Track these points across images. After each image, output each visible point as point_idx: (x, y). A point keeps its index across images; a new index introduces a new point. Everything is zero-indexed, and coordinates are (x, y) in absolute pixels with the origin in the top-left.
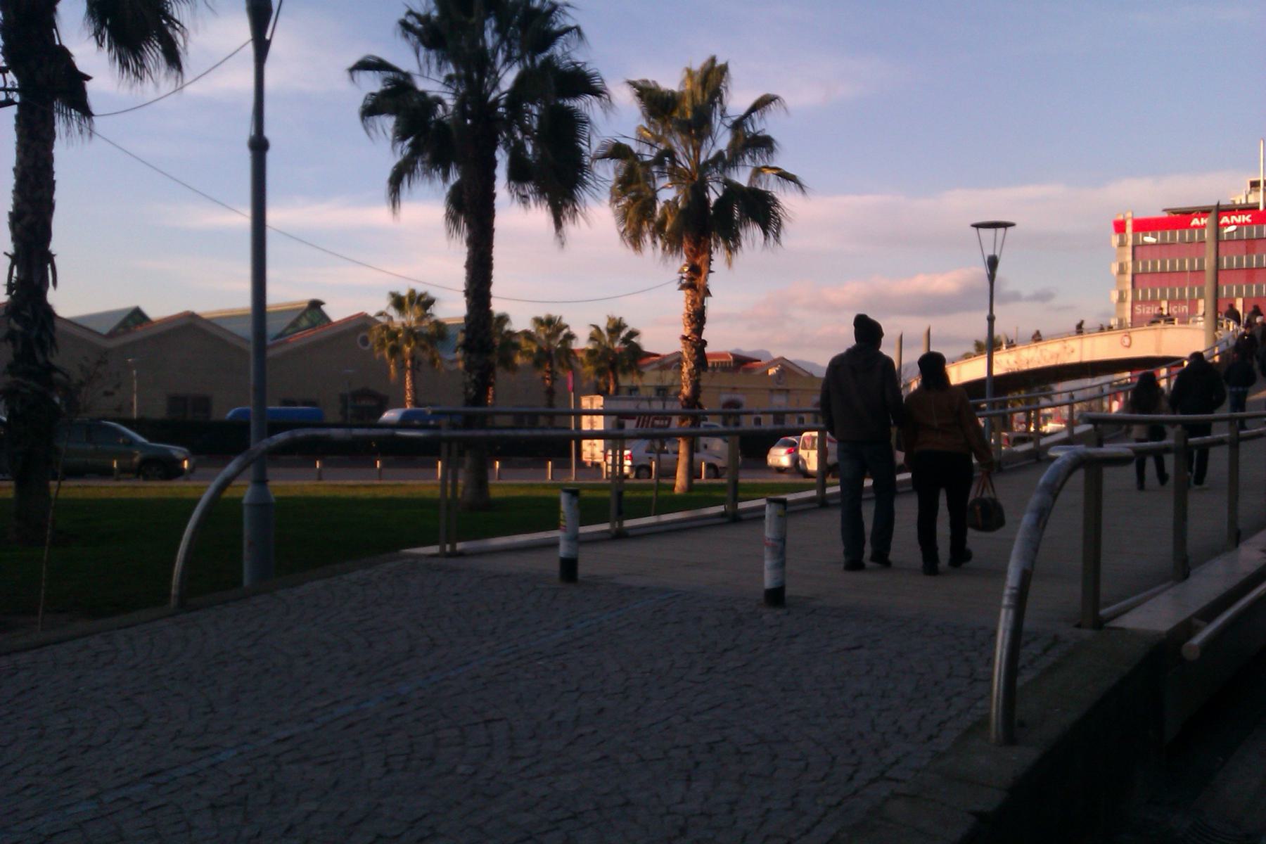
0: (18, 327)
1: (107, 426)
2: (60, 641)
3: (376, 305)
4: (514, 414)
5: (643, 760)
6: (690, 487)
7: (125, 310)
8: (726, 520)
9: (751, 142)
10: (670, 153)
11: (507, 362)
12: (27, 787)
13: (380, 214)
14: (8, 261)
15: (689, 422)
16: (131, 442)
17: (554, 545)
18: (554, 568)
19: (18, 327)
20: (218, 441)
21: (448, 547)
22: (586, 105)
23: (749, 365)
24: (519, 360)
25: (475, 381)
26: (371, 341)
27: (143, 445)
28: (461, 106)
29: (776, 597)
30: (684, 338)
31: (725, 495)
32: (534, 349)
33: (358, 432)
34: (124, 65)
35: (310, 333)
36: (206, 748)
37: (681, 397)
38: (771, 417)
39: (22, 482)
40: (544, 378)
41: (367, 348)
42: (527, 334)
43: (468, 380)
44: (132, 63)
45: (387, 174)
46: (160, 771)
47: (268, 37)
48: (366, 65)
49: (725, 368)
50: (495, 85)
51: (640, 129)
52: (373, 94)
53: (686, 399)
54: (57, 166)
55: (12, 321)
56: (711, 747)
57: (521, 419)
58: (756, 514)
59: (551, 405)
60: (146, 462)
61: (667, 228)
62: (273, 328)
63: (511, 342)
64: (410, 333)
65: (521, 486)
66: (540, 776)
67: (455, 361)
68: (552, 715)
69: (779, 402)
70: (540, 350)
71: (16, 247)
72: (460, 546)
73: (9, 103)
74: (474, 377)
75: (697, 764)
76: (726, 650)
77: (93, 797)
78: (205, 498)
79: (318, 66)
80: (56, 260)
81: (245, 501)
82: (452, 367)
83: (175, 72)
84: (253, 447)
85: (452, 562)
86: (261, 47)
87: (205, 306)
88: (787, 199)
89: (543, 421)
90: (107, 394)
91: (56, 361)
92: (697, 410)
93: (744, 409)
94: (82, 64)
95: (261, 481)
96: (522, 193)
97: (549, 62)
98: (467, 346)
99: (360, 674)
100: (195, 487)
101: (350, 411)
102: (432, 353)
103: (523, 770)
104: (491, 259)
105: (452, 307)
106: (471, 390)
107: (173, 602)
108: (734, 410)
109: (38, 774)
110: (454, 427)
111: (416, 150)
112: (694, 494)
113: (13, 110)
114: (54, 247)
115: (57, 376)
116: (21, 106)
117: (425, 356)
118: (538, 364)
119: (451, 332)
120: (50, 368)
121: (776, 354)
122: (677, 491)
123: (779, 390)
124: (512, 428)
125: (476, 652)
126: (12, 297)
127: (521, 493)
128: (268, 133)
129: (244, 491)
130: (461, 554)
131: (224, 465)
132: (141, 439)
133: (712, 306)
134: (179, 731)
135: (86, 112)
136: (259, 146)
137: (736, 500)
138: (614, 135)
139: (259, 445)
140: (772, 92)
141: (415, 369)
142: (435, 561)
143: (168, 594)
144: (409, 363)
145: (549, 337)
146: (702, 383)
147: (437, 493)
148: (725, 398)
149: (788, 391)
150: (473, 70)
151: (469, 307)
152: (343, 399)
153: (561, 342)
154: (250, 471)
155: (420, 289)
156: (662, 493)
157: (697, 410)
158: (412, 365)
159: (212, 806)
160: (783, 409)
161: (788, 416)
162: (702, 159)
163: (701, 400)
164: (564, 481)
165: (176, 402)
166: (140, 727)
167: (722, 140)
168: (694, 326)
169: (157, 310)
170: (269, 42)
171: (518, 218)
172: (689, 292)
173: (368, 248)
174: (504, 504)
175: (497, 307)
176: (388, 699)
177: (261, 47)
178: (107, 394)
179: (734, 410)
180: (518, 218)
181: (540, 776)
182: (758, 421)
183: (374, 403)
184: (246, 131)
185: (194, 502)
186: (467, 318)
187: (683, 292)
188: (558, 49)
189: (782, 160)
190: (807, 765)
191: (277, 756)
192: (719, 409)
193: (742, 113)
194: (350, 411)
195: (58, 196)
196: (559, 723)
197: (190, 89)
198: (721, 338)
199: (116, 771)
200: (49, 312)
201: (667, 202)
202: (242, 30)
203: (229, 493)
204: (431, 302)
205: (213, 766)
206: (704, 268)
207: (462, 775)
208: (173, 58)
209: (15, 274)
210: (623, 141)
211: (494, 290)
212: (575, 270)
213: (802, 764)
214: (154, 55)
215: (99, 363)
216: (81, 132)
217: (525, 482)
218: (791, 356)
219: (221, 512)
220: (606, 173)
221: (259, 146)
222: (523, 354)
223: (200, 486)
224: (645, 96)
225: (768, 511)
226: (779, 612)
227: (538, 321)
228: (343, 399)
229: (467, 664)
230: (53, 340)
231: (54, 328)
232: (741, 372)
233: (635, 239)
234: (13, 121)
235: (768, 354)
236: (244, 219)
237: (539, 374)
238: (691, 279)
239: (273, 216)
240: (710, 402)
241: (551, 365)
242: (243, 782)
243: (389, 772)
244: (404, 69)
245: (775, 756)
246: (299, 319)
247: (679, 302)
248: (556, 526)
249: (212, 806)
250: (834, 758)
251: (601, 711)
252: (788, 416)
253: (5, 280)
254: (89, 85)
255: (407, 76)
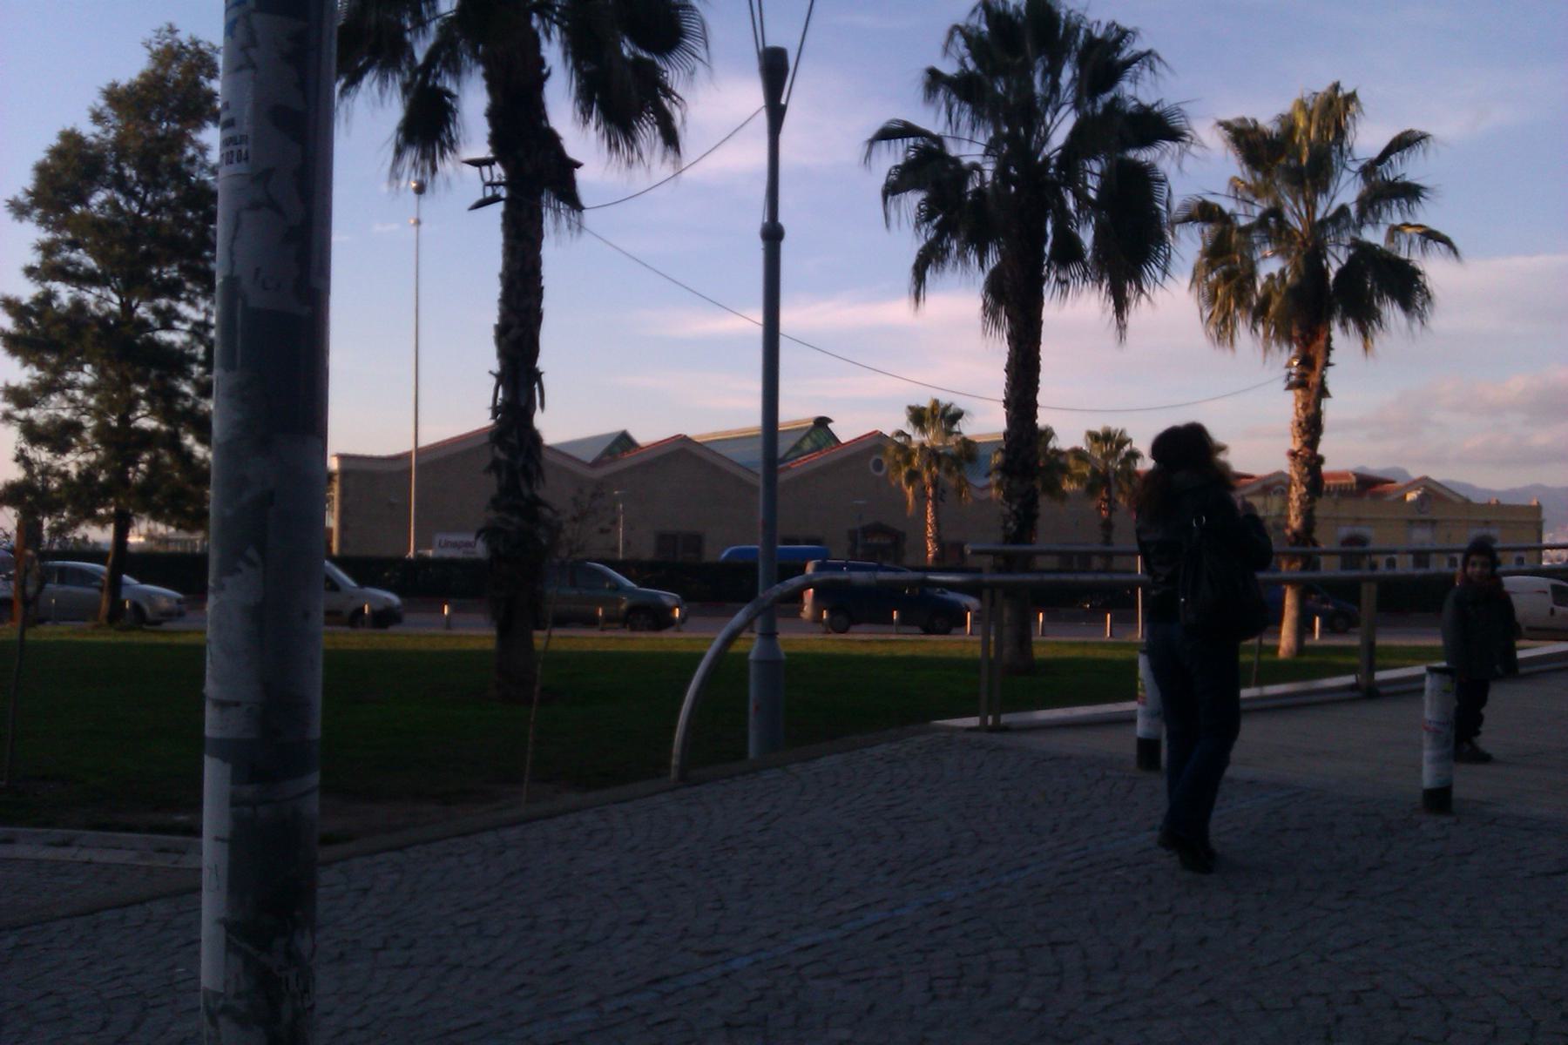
0: (502, 456)
1: (596, 571)
2: (550, 816)
3: (894, 422)
4: (1059, 553)
5: (1264, 1009)
6: (1300, 649)
7: (609, 435)
8: (1356, 694)
9: (1386, 191)
10: (1276, 212)
11: (1053, 489)
12: (522, 986)
13: (899, 310)
14: (493, 381)
15: (1299, 564)
16: (618, 587)
17: (1130, 720)
18: (1131, 750)
19: (502, 456)
20: (720, 586)
21: (990, 720)
22: (1160, 157)
23: (1379, 489)
24: (1069, 486)
25: (1015, 512)
26: (885, 463)
27: (631, 590)
28: (1001, 172)
29: (1439, 800)
30: (1293, 454)
31: (1354, 661)
32: (1086, 470)
33: (882, 576)
34: (613, 146)
35: (816, 457)
36: (719, 952)
37: (1288, 532)
38: (1410, 557)
39: (506, 629)
40: (1099, 508)
41: (882, 473)
42: (1077, 453)
43: (1007, 511)
44: (623, 145)
45: (911, 260)
46: (667, 978)
47: (783, 102)
48: (888, 134)
49: (1344, 492)
50: (1045, 141)
51: (1234, 183)
52: (896, 167)
53: (1295, 534)
54: (546, 271)
55: (497, 449)
56: (1356, 998)
57: (1066, 557)
58: (1415, 686)
59: (1107, 540)
60: (633, 610)
61: (1272, 309)
62: (784, 446)
63: (1059, 463)
64: (933, 455)
65: (1072, 645)
66: (1127, 1019)
67: (989, 487)
68: (1138, 941)
69: (1421, 537)
70: (1095, 472)
71: (503, 367)
72: (1005, 719)
73: (495, 199)
74: (1014, 507)
75: (1339, 1019)
76: (1370, 869)
77: (591, 1004)
78: (710, 653)
79: (838, 131)
80: (544, 378)
81: (751, 657)
82: (984, 495)
83: (671, 155)
84: (761, 595)
85: (997, 738)
86: (776, 114)
87: (698, 428)
88: (1434, 268)
89: (1097, 562)
90: (602, 531)
91: (541, 493)
92: (1310, 549)
93: (1370, 547)
94: (572, 149)
95: (769, 634)
96: (1062, 276)
97: (1114, 106)
98: (1006, 469)
99: (892, 872)
100: (688, 640)
101: (859, 551)
102: (960, 478)
103: (1105, 1009)
104: (1039, 358)
105: (987, 420)
106: (1011, 524)
107: (674, 774)
108: (1357, 548)
109: (531, 972)
110: (999, 570)
111: (942, 230)
112: (1306, 659)
113: (499, 208)
114: (542, 363)
115: (547, 513)
116: (509, 202)
117: (952, 482)
118: (1091, 490)
119: (982, 452)
120: (537, 502)
121: (1415, 473)
122: (1282, 654)
123: (1423, 521)
124: (1060, 571)
125: (1033, 854)
126: (498, 422)
127: (1075, 653)
128: (783, 219)
129: (751, 646)
130: (1006, 729)
131: (732, 614)
132: (629, 583)
133: (1329, 409)
134: (686, 930)
135: (575, 204)
136: (773, 235)
137: (1372, 668)
138: (1200, 192)
139: (768, 592)
140: (1418, 126)
141: (938, 498)
142: (974, 737)
143: (667, 765)
144: (930, 491)
145: (1106, 456)
146: (1317, 513)
147: (978, 651)
148: (1344, 532)
149: (1434, 522)
150: (1016, 121)
151: (1009, 420)
152: (853, 535)
153: (1123, 462)
154: (758, 625)
155: (945, 399)
156: (1266, 657)
157: (1310, 549)
158: (935, 494)
159: (727, 1025)
160: (1427, 547)
161: (1434, 556)
162: (1319, 216)
163: (1316, 535)
164: (1127, 639)
165: (665, 540)
166: (641, 922)
167: (1347, 191)
168: (1306, 438)
169: (645, 435)
170: (784, 108)
171: (1073, 311)
172: (1299, 392)
173: (900, 350)
174: (1050, 667)
175: (1043, 420)
176: (928, 905)
177: (776, 114)
178: (602, 531)
179: (1357, 548)
180: (1073, 311)
181: (1127, 1019)
182: (1391, 564)
183: (888, 541)
184: (759, 218)
185: (701, 656)
186: (1006, 434)
187: (1291, 395)
188: (1126, 88)
189: (1426, 214)
190: (1496, 1031)
191: (799, 968)
192: (1335, 546)
193: (1375, 154)
194: (859, 551)
195: (546, 305)
196: (1148, 953)
197: (685, 174)
198: (1341, 454)
199: (616, 975)
200: (535, 438)
201: (1271, 277)
202: (752, 96)
203: (738, 647)
204: (959, 415)
205: (726, 975)
206: (1319, 362)
207: (1026, 1009)
208: (671, 138)
209: (500, 395)
210: (1211, 199)
211: (1041, 398)
212: (1143, 365)
213: (1488, 1028)
214: (648, 134)
215: (594, 496)
216: (570, 227)
217: (1078, 639)
218: (1438, 475)
219: (727, 667)
220: (1188, 245)
221: (773, 235)
222: (1071, 478)
223: (701, 637)
224: (1242, 140)
225: (1429, 683)
226: (1445, 820)
227: (1094, 437)
228: (853, 535)
229: (1024, 868)
230: (540, 470)
231: (540, 456)
232: (1367, 498)
233: (1223, 329)
234: (499, 221)
235: (1404, 473)
236: (752, 321)
237: (1093, 505)
238: (1302, 376)
239: (788, 319)
240: (1328, 538)
241: (1109, 492)
242: (761, 998)
243: (935, 998)
244: (935, 132)
245: (1448, 1015)
246: (802, 440)
247: (1286, 407)
248: (1131, 695)
249: (727, 1025)
250: (1536, 1023)
251: (1203, 941)
252: (1434, 556)
253: (490, 403)
254: (579, 174)
255: (938, 140)
